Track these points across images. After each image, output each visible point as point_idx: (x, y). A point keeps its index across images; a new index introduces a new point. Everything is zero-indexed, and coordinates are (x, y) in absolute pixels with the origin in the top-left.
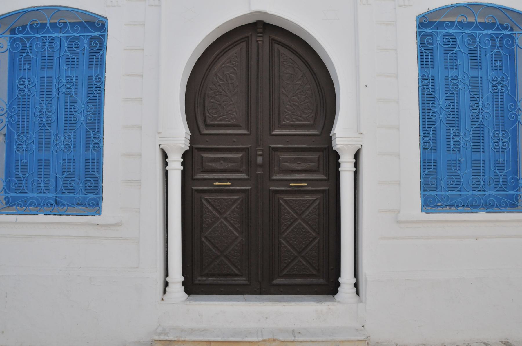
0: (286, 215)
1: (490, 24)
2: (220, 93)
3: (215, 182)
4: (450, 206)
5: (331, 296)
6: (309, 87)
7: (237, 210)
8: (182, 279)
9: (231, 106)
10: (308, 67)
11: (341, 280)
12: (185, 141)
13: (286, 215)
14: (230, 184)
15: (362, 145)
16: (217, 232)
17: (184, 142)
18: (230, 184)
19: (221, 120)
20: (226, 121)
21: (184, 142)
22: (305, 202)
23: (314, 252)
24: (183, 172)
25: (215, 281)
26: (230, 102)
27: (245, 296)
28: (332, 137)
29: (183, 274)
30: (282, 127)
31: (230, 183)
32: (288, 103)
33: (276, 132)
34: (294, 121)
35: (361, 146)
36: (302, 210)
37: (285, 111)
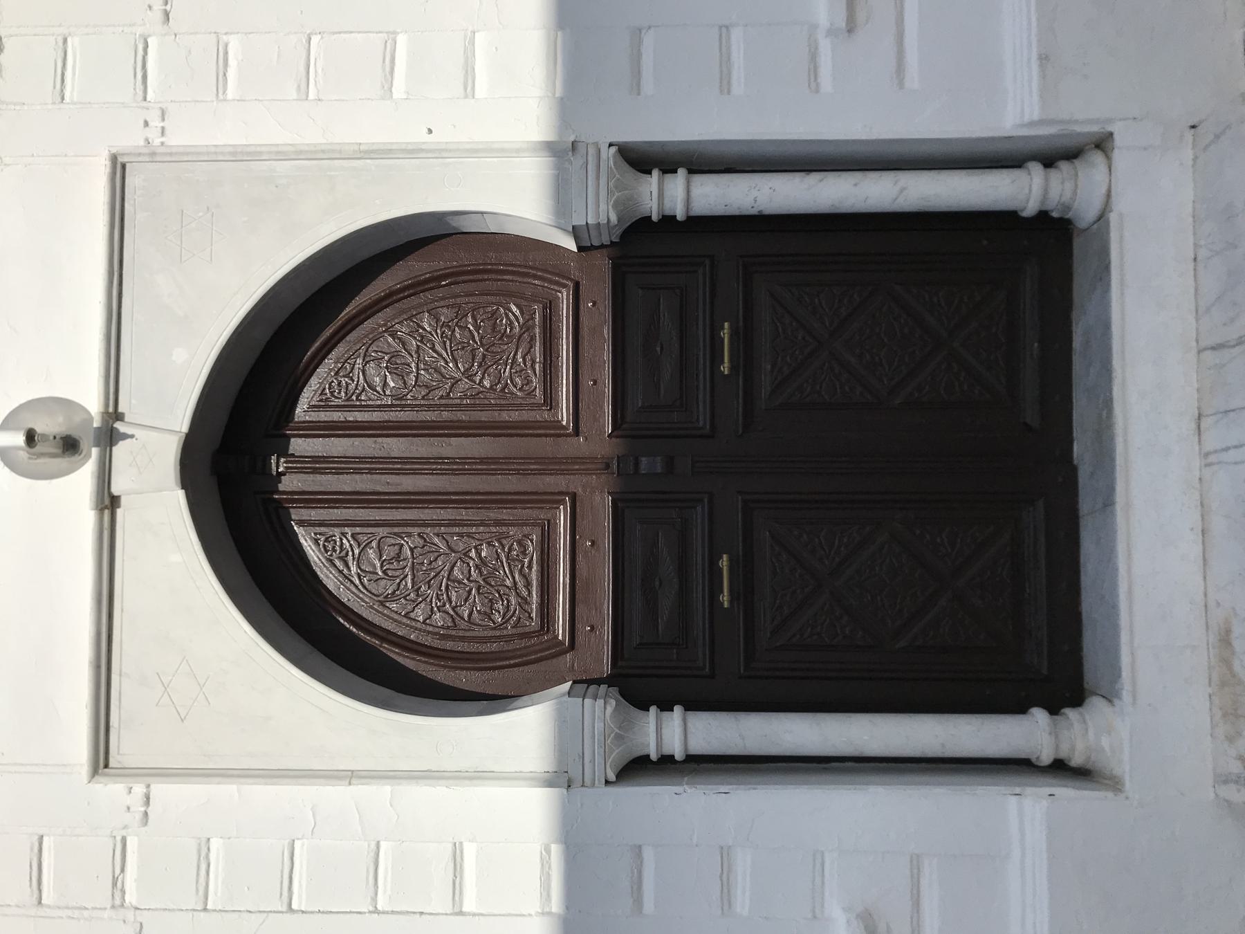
0: (821, 387)
1: (347, 628)
2: (443, 588)
3: (722, 604)
4: (113, 439)
5: (1077, 243)
6: (426, 315)
7: (805, 536)
8: (1039, 715)
9: (483, 554)
10: (356, 321)
11: (1030, 209)
12: (595, 698)
13: (821, 387)
14: (725, 557)
15: (611, 145)
16: (879, 598)
17: (600, 702)
18: (725, 557)
19: (528, 585)
20: (530, 567)
21: (600, 702)
22: (780, 330)
23: (935, 300)
24: (693, 705)
25: (354, 311)
26: (471, 558)
27: (1081, 513)
28: (580, 245)
29: (1020, 708)
30: (550, 401)
31: (721, 557)
32: (478, 379)
33: (564, 415)
34: (534, 362)
35: (611, 148)
36: (804, 338)
37: (503, 390)
